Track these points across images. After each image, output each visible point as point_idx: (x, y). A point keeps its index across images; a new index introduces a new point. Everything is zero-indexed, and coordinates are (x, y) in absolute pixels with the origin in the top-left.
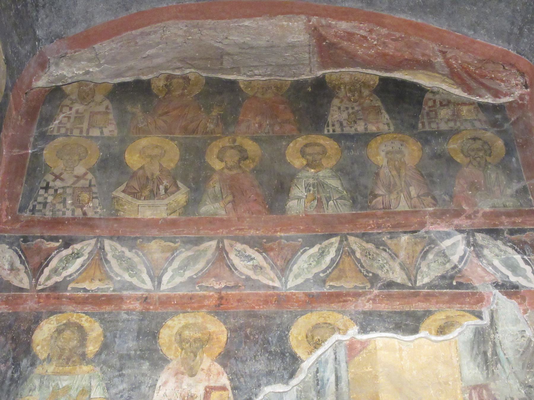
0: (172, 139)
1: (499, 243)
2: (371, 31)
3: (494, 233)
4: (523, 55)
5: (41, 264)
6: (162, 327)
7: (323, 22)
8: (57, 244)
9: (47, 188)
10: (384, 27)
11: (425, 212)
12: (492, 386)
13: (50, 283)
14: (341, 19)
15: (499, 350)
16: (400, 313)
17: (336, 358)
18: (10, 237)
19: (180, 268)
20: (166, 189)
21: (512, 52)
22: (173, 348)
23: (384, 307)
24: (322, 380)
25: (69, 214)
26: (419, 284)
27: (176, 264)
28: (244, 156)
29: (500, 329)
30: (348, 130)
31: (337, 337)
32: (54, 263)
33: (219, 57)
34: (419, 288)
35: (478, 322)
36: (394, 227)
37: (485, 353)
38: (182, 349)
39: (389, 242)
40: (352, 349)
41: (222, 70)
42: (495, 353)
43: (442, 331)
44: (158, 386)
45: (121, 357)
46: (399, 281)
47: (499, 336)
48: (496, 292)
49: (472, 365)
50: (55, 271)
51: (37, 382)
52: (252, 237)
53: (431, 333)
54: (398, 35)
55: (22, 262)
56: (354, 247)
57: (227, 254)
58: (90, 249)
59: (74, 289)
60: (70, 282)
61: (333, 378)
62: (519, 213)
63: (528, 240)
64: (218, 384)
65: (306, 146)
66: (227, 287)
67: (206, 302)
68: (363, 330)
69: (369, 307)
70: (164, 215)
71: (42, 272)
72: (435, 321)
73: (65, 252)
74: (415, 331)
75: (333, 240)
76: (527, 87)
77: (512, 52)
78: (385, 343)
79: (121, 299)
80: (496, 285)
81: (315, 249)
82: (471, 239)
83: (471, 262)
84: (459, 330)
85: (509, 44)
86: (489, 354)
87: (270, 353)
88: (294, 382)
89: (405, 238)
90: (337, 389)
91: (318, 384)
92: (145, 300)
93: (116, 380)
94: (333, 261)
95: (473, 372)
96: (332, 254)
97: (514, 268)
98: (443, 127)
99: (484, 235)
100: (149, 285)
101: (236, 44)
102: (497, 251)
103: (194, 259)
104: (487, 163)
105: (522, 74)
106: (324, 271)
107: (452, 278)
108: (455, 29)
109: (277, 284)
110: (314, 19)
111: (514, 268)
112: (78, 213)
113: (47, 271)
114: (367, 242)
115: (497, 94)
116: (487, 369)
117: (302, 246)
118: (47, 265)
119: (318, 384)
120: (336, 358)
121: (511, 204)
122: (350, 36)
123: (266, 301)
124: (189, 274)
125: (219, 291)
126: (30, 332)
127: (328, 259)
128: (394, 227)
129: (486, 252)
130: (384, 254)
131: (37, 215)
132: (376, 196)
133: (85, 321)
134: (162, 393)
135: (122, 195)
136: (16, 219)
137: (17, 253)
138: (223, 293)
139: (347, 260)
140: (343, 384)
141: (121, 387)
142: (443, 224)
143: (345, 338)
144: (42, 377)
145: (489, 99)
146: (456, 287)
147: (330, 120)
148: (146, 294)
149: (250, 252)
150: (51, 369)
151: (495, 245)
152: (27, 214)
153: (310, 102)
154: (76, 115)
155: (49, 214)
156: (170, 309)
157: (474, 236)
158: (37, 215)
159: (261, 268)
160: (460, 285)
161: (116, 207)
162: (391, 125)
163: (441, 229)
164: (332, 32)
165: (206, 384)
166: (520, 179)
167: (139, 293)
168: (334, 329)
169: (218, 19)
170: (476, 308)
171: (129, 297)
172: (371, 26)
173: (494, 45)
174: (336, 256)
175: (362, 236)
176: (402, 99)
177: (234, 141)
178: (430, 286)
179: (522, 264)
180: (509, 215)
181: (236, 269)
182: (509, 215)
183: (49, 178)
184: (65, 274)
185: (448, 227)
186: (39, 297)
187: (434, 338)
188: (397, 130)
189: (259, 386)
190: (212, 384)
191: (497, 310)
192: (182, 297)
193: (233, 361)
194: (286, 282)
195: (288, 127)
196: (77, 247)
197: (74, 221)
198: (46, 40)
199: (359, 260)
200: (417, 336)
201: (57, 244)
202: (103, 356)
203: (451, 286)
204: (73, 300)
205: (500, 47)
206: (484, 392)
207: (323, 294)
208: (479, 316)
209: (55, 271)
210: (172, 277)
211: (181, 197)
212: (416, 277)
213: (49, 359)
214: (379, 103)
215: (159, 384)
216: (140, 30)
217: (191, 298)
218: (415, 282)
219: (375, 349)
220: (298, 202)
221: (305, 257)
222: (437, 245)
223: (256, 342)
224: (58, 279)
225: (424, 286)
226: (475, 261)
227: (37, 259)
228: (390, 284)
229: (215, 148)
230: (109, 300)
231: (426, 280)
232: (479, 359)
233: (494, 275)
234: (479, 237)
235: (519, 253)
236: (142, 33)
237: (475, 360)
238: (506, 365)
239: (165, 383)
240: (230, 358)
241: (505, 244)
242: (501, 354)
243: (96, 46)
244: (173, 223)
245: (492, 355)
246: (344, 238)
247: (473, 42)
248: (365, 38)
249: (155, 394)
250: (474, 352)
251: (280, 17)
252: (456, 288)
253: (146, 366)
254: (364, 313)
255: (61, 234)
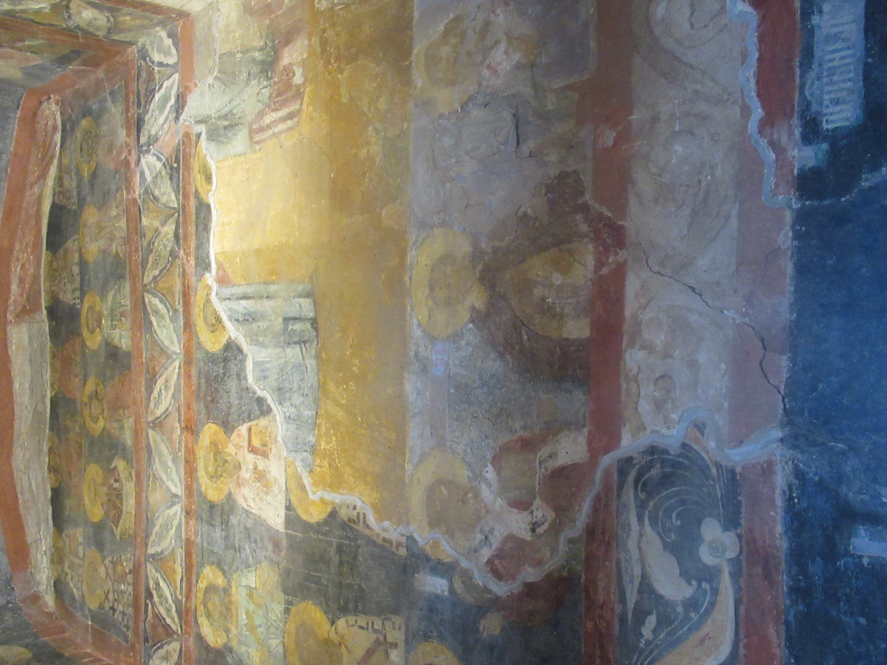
0: (85, 470)
1: (146, 118)
2: (18, 259)
3: (139, 124)
4: (19, 102)
5: (163, 625)
6: (206, 497)
7: (12, 308)
8: (150, 605)
9: (113, 609)
10: (13, 245)
11: (128, 199)
12: (249, 118)
13: (176, 619)
14: (9, 290)
15: (223, 112)
16: (197, 225)
17: (229, 299)
18: (145, 657)
19: (166, 473)
20: (116, 481)
21: (18, 114)
22: (221, 486)
23: (193, 244)
24: (244, 315)
25: (130, 589)
26: (176, 206)
27: (164, 477)
28: (95, 395)
29: (208, 113)
30: (77, 284)
31: (213, 298)
32: (164, 613)
33: (37, 414)
34: (179, 204)
35: (204, 136)
36: (137, 234)
37: (226, 128)
38: (222, 476)
39: (148, 239)
40: (223, 280)
41: (45, 412)
42: (225, 117)
43: (209, 179)
44: (247, 508)
45: (227, 547)
46: (174, 227)
47: (213, 113)
48: (181, 118)
49: (234, 143)
50: (168, 611)
51: (243, 649)
52: (146, 390)
53: (210, 191)
54: (19, 233)
55: (161, 647)
56: (151, 277)
57: (157, 418)
58: (154, 571)
59: (181, 593)
60: (176, 596)
61: (244, 303)
62: (127, 97)
63: (145, 87)
64: (246, 436)
65: (88, 328)
66: (179, 421)
67: (190, 445)
68: (208, 267)
69: (193, 262)
70: (133, 484)
71: (169, 625)
72: (202, 185)
73: (156, 599)
74: (208, 207)
75: (147, 300)
76: (50, 98)
77: (18, 114)
78: (218, 244)
79: (188, 540)
80: (177, 118)
81: (153, 319)
82: (144, 148)
83: (161, 147)
84: (209, 159)
85: (10, 117)
86: (226, 123)
87: (224, 374)
88: (245, 348)
89: (145, 222)
90: (253, 298)
91: (248, 320)
92: (188, 513)
93: (243, 555)
94: (161, 301)
95: (239, 141)
96: (156, 301)
97: (166, 100)
98: (74, 183)
99: (141, 135)
100: (177, 508)
101: (30, 398)
102: (152, 120)
103: (161, 455)
104: (96, 136)
105: (41, 103)
106: (169, 312)
107: (172, 168)
108: (4, 174)
109: (177, 364)
110: (10, 317)
111: (166, 100)
112: (130, 578)
113: (169, 621)
114: (148, 262)
115: (55, 128)
116: (237, 125)
117: (152, 335)
118: (164, 619)
119: (248, 320)
120: (229, 299)
121: (121, 107)
122: (22, 281)
123: (188, 376)
124: (170, 464)
125: (182, 429)
126: (207, 648)
127: (160, 306)
128: (137, 234)
129: (153, 132)
130: (156, 244)
131: (131, 624)
132: (117, 253)
133: (202, 585)
134: (252, 504)
135: (119, 529)
136: (132, 648)
137: (155, 651)
138: (183, 425)
139: (161, 285)
140: (250, 290)
141: (248, 551)
142: (134, 179)
143: (215, 287)
144: (240, 642)
145: (58, 137)
146: (179, 165)
147: (72, 302)
148: (184, 513)
149: (155, 394)
150: (234, 631)
151: (148, 123)
152: (130, 634)
153: (63, 321)
154: (394, 544)
155: (130, 611)
156: (195, 486)
157: (142, 146)
158: (131, 624)
159: (167, 381)
160: (177, 160)
161: (127, 536)
162: (73, 238)
163: (138, 182)
164: (19, 299)
165: (246, 450)
166: (105, 100)
167: (183, 519)
168: (208, 301)
169: (13, 414)
170: (194, 138)
171: (186, 534)
172: (13, 259)
173: (15, 133)
174: (158, 297)
175: (144, 268)
176: (61, 227)
177: (86, 404)
178: (177, 193)
179: (162, 91)
180: (127, 110)
181: (167, 409)
182: (127, 110)
183: (107, 606)
184: (170, 601)
185: (135, 173)
186: (186, 633)
187: (214, 187)
188: (76, 231)
189: (247, 388)
190: (246, 444)
191: (195, 117)
192: (186, 473)
193: (230, 419)
194: (176, 353)
195: (77, 348)
196: (152, 584)
197: (135, 585)
198: (9, 595)
199: (161, 271)
200: (212, 206)
201: (150, 605)
202: (226, 568)
203: (178, 168)
204: (188, 598)
205: (16, 127)
206: (254, 127)
207: (184, 311)
208: (199, 136)
209: (168, 611)
210: (173, 481)
211: (120, 464)
212: (171, 208)
213: (227, 631)
214: (61, 250)
215: (245, 506)
216: (19, 496)
217: (187, 462)
218: (174, 208)
219: (222, 253)
220: (123, 339)
221: (159, 332)
222: (149, 186)
223: (216, 389)
224: (174, 609)
225: (178, 199)
226: (160, 143)
227: (160, 630)
228: (176, 236)
229: (91, 425)
230: (188, 555)
231: (173, 197)
232: (229, 134)
233: (170, 122)
234: (143, 140)
235: (154, 96)
236: (22, 494)
237: (230, 139)
238: (235, 103)
239: (245, 498)
240: (228, 421)
241: (147, 112)
242: (227, 109)
243: (29, 542)
244: (138, 475)
245: (227, 120)
246: (145, 287)
247: (15, 154)
248: (23, 265)
249: (253, 511)
250: (225, 140)
251: (9, 352)
252: (179, 165)
253: (234, 520)
254: (196, 265)
255: (143, 602)
